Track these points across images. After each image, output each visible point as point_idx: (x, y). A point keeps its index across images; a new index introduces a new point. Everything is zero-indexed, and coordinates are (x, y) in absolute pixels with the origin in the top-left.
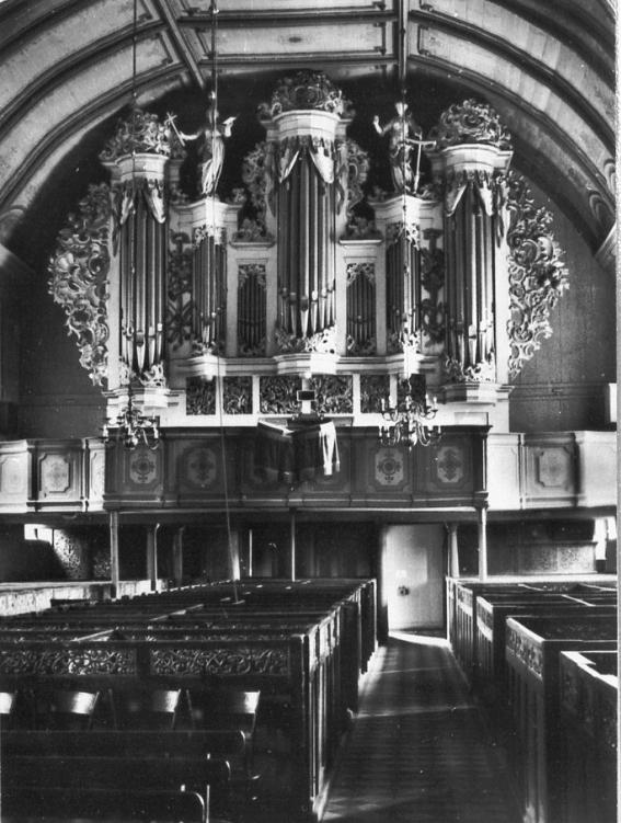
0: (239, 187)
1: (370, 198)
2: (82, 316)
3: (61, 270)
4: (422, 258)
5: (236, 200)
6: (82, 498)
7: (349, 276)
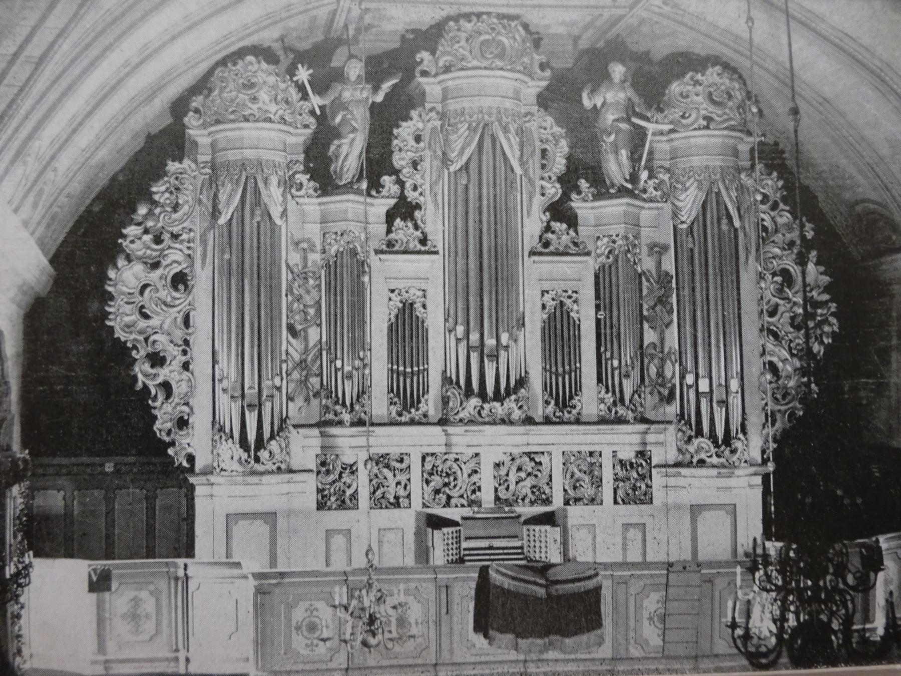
0: (390, 175)
1: (574, 196)
2: (157, 360)
3: (125, 289)
4: (645, 283)
5: (384, 192)
6: (177, 650)
7: (544, 307)
